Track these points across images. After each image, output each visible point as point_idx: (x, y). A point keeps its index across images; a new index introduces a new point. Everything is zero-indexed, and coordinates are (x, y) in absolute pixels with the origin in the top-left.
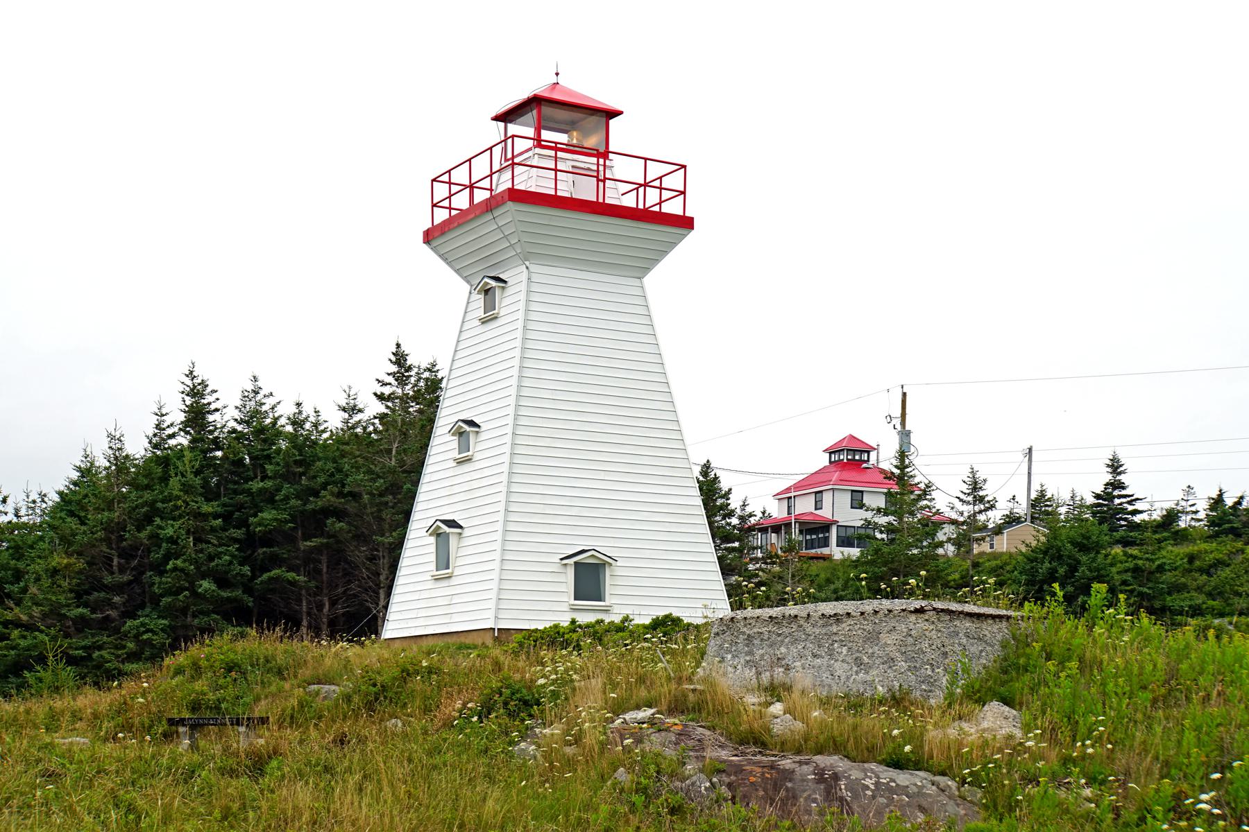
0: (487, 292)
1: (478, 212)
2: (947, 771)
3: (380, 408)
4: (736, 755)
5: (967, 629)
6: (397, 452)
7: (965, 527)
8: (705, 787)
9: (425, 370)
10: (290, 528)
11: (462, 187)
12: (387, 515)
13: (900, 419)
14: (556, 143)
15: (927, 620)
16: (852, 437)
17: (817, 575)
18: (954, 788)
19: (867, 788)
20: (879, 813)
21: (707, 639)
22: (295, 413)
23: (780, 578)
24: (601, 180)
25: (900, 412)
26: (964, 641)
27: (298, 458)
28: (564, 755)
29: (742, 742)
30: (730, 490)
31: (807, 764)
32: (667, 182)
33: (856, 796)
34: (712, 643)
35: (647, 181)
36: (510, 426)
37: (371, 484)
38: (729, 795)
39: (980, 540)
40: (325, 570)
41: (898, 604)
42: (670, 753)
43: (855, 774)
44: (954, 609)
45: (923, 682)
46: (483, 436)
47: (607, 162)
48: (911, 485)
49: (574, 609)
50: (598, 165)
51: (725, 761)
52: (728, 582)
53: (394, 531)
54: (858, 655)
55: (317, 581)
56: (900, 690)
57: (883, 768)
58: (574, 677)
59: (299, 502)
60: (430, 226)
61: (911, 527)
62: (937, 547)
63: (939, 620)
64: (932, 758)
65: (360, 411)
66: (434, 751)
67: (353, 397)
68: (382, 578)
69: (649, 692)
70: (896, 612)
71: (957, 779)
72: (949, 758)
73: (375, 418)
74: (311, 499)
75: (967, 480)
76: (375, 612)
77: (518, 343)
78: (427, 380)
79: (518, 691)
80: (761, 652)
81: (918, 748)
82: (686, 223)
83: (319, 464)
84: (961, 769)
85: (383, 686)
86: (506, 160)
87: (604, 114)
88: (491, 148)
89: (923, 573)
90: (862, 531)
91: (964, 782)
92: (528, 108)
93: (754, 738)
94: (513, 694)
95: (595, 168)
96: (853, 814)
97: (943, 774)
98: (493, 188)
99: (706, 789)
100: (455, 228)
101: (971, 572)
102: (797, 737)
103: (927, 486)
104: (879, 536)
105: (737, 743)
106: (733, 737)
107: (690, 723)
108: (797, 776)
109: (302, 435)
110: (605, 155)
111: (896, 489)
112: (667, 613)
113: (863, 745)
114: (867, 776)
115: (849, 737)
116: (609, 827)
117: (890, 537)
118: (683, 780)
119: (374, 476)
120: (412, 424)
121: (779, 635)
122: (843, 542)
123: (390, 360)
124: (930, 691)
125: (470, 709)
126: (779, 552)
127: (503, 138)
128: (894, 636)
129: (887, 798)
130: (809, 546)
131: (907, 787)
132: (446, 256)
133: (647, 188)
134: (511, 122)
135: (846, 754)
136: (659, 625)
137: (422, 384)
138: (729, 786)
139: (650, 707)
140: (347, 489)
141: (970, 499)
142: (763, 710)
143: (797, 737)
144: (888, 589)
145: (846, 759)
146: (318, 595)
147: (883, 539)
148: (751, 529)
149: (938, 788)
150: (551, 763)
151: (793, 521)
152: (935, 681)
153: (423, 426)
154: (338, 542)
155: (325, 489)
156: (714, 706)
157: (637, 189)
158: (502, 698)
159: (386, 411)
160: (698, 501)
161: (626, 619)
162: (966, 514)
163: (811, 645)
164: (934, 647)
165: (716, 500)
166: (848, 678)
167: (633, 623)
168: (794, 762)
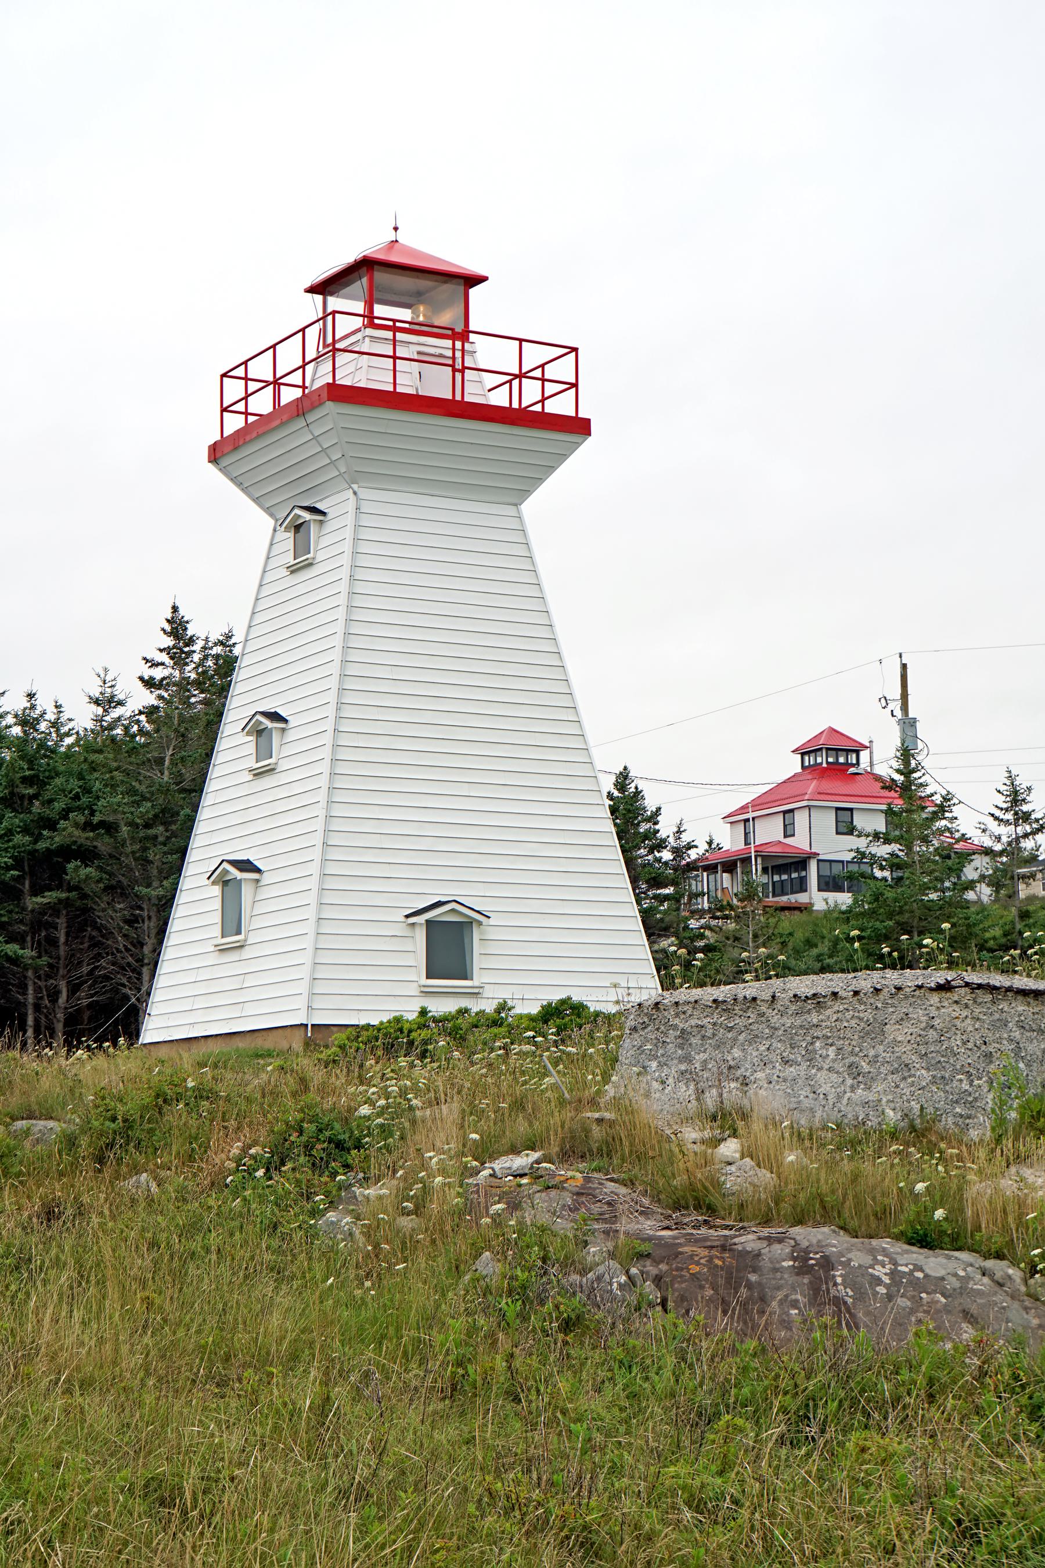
0: (298, 528)
1: (285, 417)
2: (1005, 1251)
3: (148, 698)
4: (667, 1228)
5: (1020, 1015)
6: (173, 763)
7: (1004, 859)
8: (619, 1284)
9: (216, 644)
10: (13, 878)
11: (263, 384)
12: (154, 854)
13: (900, 702)
14: (394, 321)
15: (956, 1002)
16: (833, 731)
17: (791, 934)
18: (1018, 1280)
19: (878, 1281)
20: (900, 1324)
21: (621, 1037)
22: (25, 709)
23: (737, 939)
24: (459, 370)
25: (900, 691)
26: (1017, 1034)
27: (27, 773)
28: (398, 1232)
29: (678, 1206)
30: (659, 809)
31: (780, 1241)
32: (550, 372)
33: (860, 1296)
34: (627, 1043)
35: (524, 371)
36: (331, 720)
37: (133, 809)
38: (655, 1296)
39: (1029, 877)
40: (62, 939)
41: (910, 978)
42: (563, 1225)
43: (858, 1258)
44: (998, 984)
45: (957, 1102)
46: (291, 736)
47: (467, 345)
48: (921, 798)
49: (426, 994)
50: (454, 349)
51: (650, 1239)
52: (656, 947)
53: (166, 878)
54: (852, 1059)
55: (51, 957)
56: (921, 1116)
57: (901, 1247)
58: (415, 1102)
59: (27, 838)
60: (217, 437)
61: (925, 860)
62: (966, 889)
63: (975, 1002)
64: (979, 1229)
65: (121, 703)
66: (190, 1230)
67: (109, 684)
68: (146, 950)
69: (531, 1124)
70: (908, 990)
71: (1022, 1265)
72: (1005, 1229)
73: (141, 713)
74: (45, 833)
75: (1003, 788)
76: (133, 1000)
77: (342, 600)
78: (217, 657)
79: (329, 1126)
80: (702, 1056)
81: (956, 1213)
82: (580, 427)
83: (58, 781)
84: (1028, 1248)
85: (125, 1121)
86: (325, 346)
87: (462, 281)
88: (303, 330)
89: (946, 926)
90: (854, 868)
91: (1033, 1271)
92: (356, 274)
93: (696, 1198)
94: (320, 1130)
95: (449, 353)
96: (858, 1328)
97: (999, 1256)
98: (307, 384)
99: (621, 1286)
100: (251, 440)
101: (1019, 926)
102: (763, 1196)
103: (946, 799)
104: (878, 874)
105: (668, 1207)
106: (662, 1197)
107: (596, 1175)
108: (765, 1263)
109: (34, 739)
110: (464, 335)
111: (898, 804)
112: (563, 996)
113: (869, 1209)
114: (876, 1261)
115: (845, 1196)
116: (464, 1356)
117: (895, 875)
118: (583, 1272)
119: (137, 798)
120: (194, 719)
121: (730, 1029)
122: (827, 884)
123: (163, 630)
124: (969, 1117)
125: (253, 1157)
126: (735, 901)
127: (321, 315)
128: (908, 1028)
129: (912, 1298)
130: (778, 890)
131: (943, 1279)
132: (240, 479)
133: (523, 380)
134: (332, 294)
135: (842, 1223)
136: (552, 1015)
137: (210, 663)
138: (658, 1280)
139: (533, 1149)
140: (96, 819)
141: (1009, 816)
142: (710, 1151)
143: (763, 1196)
144: (895, 954)
145: (842, 1233)
146: (51, 978)
147: (885, 879)
148: (692, 867)
149: (993, 1280)
150: (376, 1246)
151: (753, 855)
152: (976, 1099)
153: (209, 723)
154: (84, 896)
155: (66, 818)
156: (631, 1145)
157: (510, 382)
158: (304, 1138)
159: (155, 703)
160: (609, 826)
161: (503, 1007)
162: (1004, 839)
163: (779, 1045)
164: (970, 1045)
165: (638, 824)
166: (839, 1097)
167: (512, 1013)
168: (760, 1239)
